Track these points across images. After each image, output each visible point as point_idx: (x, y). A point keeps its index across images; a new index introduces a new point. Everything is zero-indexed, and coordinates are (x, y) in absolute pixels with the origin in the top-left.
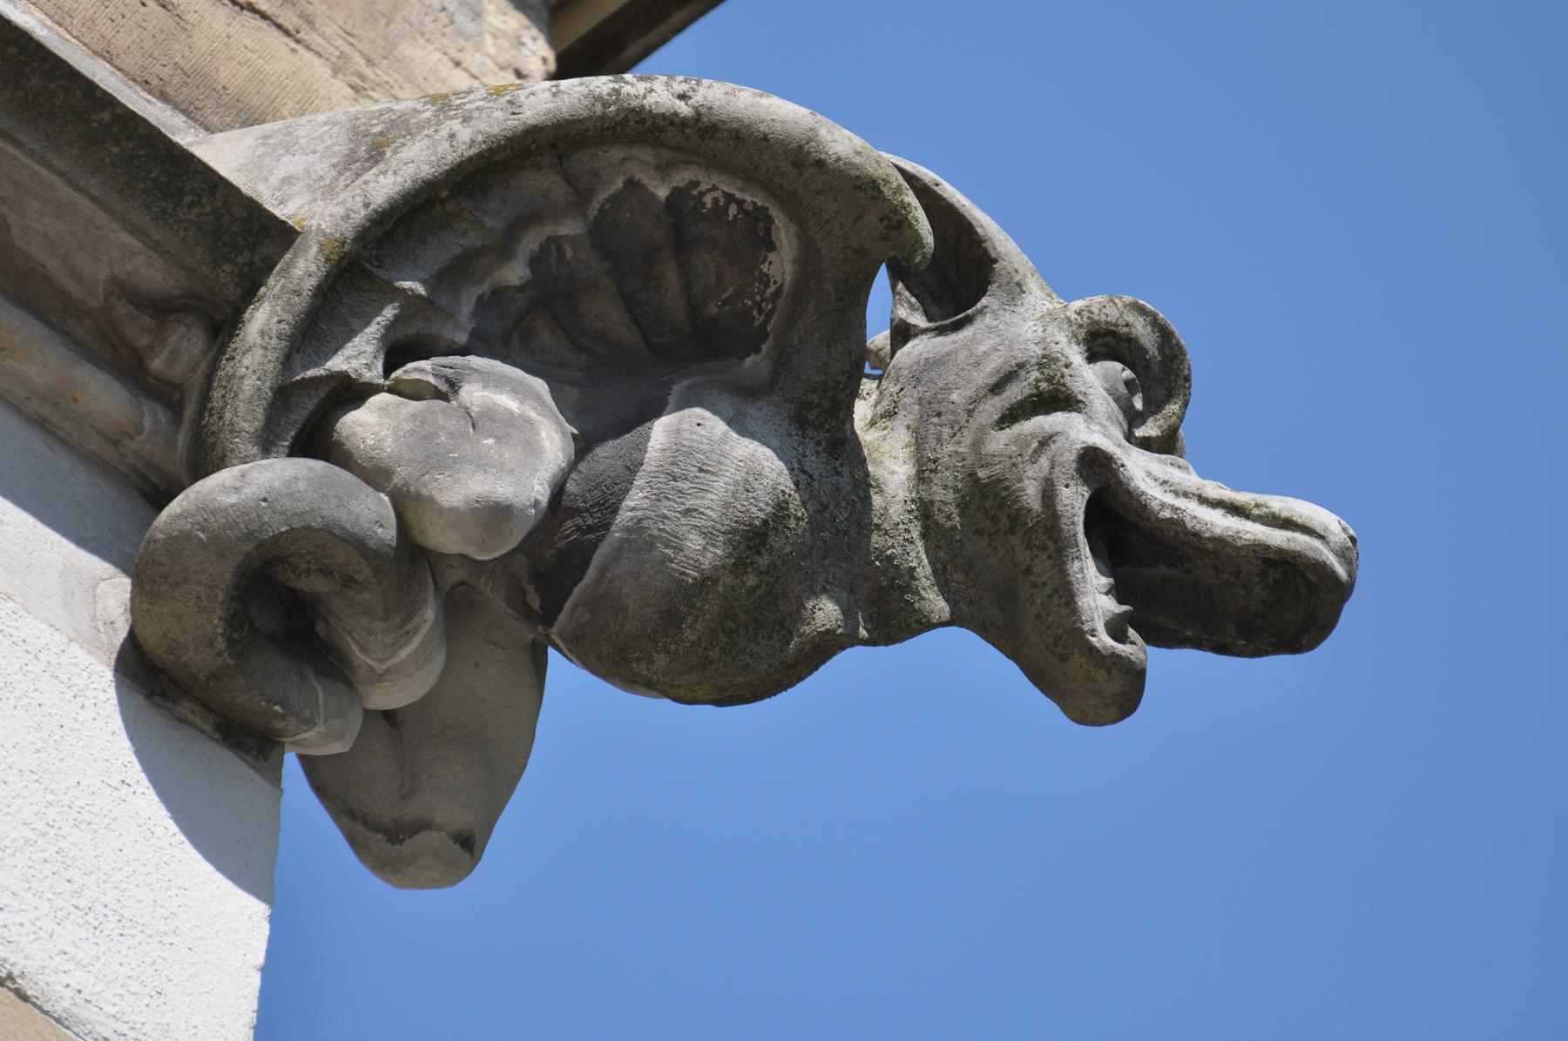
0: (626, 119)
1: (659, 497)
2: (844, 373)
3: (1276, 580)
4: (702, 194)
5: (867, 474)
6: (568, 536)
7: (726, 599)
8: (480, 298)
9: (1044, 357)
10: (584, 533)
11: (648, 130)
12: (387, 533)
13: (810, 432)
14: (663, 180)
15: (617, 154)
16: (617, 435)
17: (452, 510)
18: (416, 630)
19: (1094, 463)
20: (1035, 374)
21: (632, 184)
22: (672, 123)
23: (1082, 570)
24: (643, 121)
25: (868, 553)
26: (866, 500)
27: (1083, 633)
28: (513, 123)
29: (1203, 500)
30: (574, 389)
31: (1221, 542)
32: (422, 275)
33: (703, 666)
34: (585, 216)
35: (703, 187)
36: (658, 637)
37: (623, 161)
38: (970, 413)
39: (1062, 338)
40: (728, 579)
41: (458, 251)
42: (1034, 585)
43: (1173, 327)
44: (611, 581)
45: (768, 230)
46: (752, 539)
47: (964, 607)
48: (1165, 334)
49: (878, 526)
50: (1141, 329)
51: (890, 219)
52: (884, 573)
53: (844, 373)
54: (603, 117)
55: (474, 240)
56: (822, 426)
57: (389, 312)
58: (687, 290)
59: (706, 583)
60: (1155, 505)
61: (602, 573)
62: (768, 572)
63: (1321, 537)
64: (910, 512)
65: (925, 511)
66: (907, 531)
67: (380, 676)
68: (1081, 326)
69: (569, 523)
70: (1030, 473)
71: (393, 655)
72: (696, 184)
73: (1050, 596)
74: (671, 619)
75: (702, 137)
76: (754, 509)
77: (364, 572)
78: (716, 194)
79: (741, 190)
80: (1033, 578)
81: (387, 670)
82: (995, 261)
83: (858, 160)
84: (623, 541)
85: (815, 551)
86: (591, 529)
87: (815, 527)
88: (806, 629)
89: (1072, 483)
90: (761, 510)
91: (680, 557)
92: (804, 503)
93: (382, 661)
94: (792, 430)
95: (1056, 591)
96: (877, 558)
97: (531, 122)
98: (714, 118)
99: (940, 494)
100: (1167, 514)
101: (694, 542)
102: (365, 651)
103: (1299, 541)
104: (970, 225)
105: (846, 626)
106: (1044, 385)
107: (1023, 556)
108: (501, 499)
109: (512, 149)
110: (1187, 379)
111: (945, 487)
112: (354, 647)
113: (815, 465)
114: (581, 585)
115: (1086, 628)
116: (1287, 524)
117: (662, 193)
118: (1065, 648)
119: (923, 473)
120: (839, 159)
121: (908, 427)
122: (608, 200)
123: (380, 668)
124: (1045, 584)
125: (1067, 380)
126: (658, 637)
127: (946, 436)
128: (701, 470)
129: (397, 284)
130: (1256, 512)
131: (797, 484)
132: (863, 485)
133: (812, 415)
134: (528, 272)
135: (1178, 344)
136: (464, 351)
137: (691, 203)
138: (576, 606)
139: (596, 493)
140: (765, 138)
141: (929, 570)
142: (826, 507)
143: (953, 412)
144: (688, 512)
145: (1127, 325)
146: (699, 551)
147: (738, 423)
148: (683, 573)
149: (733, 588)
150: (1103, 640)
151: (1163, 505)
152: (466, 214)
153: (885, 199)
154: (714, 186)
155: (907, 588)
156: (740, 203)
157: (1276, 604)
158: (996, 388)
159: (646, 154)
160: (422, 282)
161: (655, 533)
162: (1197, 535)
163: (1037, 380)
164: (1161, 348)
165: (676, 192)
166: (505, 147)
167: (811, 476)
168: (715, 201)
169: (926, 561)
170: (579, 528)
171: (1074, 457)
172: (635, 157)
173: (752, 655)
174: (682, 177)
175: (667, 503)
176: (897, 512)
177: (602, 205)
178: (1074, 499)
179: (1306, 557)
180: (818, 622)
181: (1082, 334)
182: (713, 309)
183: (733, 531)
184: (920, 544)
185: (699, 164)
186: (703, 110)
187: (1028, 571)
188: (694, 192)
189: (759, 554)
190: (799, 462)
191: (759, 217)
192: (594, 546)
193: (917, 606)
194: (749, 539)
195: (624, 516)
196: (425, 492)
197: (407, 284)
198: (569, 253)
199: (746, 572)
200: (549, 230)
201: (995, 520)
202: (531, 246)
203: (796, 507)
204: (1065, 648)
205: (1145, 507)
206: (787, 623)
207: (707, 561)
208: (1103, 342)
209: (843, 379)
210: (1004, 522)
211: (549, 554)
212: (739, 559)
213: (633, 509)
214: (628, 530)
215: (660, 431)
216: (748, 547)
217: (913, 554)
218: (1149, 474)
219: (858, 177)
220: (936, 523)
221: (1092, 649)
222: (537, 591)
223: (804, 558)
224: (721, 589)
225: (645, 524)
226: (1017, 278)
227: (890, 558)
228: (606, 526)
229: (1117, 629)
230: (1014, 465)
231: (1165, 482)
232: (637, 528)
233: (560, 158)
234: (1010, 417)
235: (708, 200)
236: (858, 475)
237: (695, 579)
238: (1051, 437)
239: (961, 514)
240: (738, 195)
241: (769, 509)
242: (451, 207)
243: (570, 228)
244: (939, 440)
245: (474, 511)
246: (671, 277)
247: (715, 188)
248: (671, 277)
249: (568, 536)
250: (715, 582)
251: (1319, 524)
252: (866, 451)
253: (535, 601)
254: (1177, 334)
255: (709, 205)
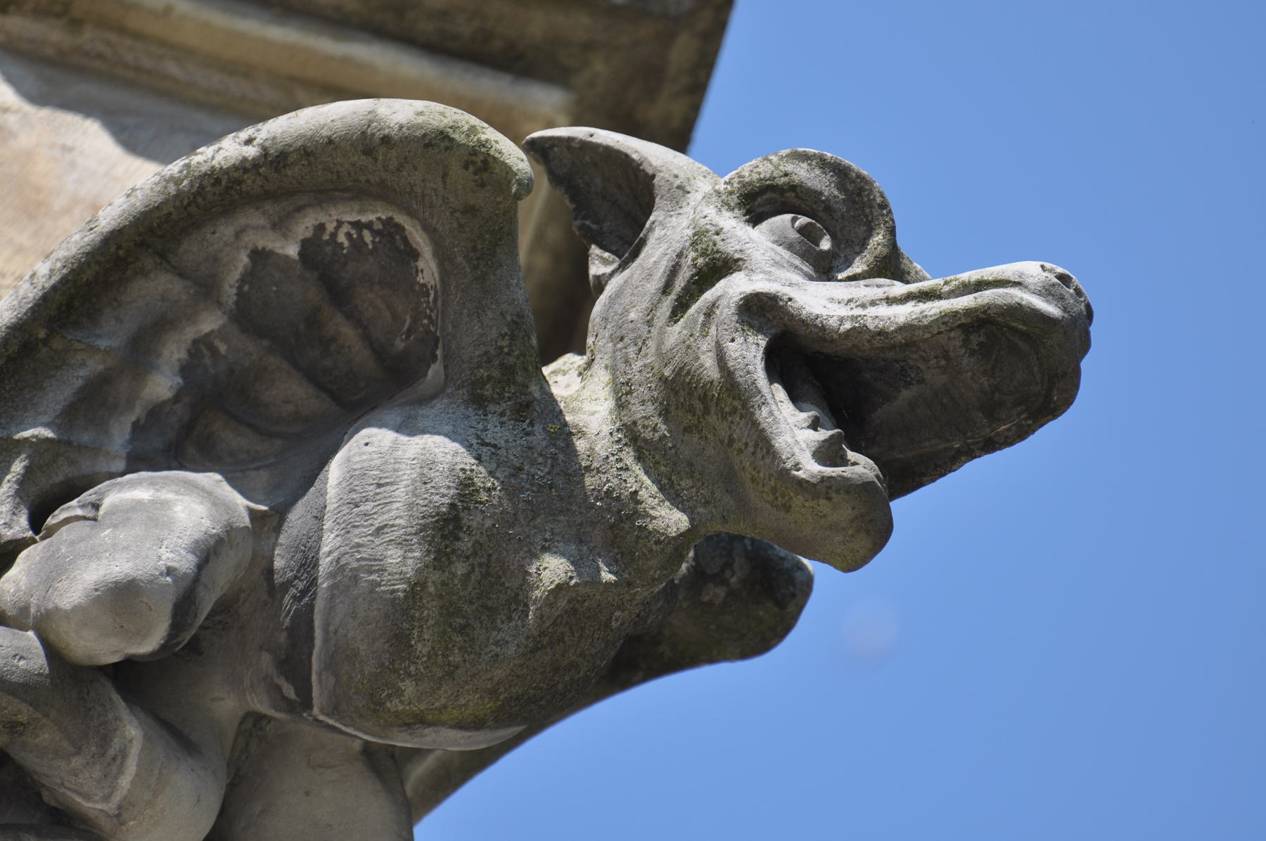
0: (202, 187)
1: (347, 529)
2: (503, 336)
3: (981, 344)
4: (334, 235)
5: (566, 424)
6: (289, 611)
7: (441, 597)
8: (135, 425)
9: (695, 235)
10: (300, 599)
11: (228, 188)
12: (37, 661)
13: (491, 408)
14: (285, 236)
15: (226, 230)
16: (304, 494)
17: (76, 609)
18: (124, 754)
19: (758, 310)
20: (692, 254)
21: (260, 256)
22: (246, 170)
23: (771, 413)
24: (218, 181)
25: (586, 497)
26: (570, 450)
27: (788, 471)
28: (90, 237)
29: (890, 301)
30: (261, 472)
31: (907, 328)
32: (45, 419)
33: (450, 674)
34: (219, 304)
35: (330, 227)
36: (397, 666)
37: (238, 235)
38: (649, 323)
39: (711, 211)
40: (436, 576)
41: (80, 383)
42: (740, 451)
43: (847, 162)
44: (336, 632)
45: (405, 240)
46: (446, 528)
47: (701, 510)
48: (840, 172)
49: (588, 469)
50: (802, 173)
51: (473, 163)
52: (609, 510)
53: (503, 336)
54: (179, 195)
55: (94, 366)
56: (501, 396)
57: (18, 467)
58: (367, 338)
59: (416, 589)
60: (833, 323)
61: (326, 631)
62: (475, 554)
63: (1017, 284)
64: (619, 441)
65: (631, 435)
66: (620, 460)
67: (118, 816)
68: (731, 193)
69: (287, 597)
70: (704, 348)
71: (113, 788)
72: (321, 228)
73: (753, 453)
74: (400, 641)
75: (277, 170)
76: (436, 498)
77: (25, 713)
78: (345, 228)
79: (362, 211)
80: (736, 445)
81: (120, 807)
82: (653, 176)
83: (420, 119)
84: (333, 587)
85: (521, 517)
86: (304, 593)
87: (511, 491)
88: (537, 593)
89: (736, 335)
90: (444, 496)
91: (386, 577)
92: (491, 473)
93: (106, 799)
94: (470, 411)
95: (756, 446)
96: (597, 499)
97: (108, 228)
98: (279, 147)
99: (643, 410)
100: (848, 326)
101: (394, 556)
102: (87, 797)
103: (987, 296)
104: (627, 156)
105: (580, 575)
106: (700, 261)
107: (723, 429)
108: (120, 577)
109: (98, 263)
110: (884, 205)
111: (643, 403)
112: (78, 799)
113: (497, 433)
114: (316, 651)
115: (789, 465)
116: (980, 285)
117: (292, 251)
118: (783, 496)
119: (622, 395)
120: (401, 127)
121: (606, 367)
122: (243, 280)
123: (110, 807)
124: (746, 445)
125: (721, 246)
126: (397, 666)
127: (632, 355)
128: (379, 486)
129: (17, 436)
130: (946, 288)
131: (478, 458)
132: (563, 435)
133: (488, 391)
134: (179, 380)
135: (859, 176)
136: (122, 474)
137: (328, 249)
138: (319, 675)
139: (299, 556)
140: (330, 141)
141: (654, 489)
142: (520, 469)
143: (633, 330)
144: (379, 531)
145: (786, 175)
146: (400, 562)
147: (408, 427)
148: (393, 591)
149: (443, 584)
150: (811, 468)
151: (842, 320)
152: (77, 345)
153: (459, 145)
154: (340, 220)
155: (636, 514)
156: (369, 226)
157: (1012, 372)
158: (666, 289)
159: (253, 218)
160: (46, 425)
161: (355, 565)
162: (882, 333)
163: (694, 260)
164: (841, 187)
165: (306, 244)
166: (88, 264)
167: (495, 446)
168: (348, 235)
169: (648, 482)
170: (294, 597)
171: (733, 310)
172: (248, 226)
173: (496, 643)
174: (304, 226)
175: (357, 531)
176: (603, 447)
177: (239, 288)
178: (748, 352)
179: (996, 306)
180: (546, 581)
181: (734, 200)
182: (400, 345)
183: (424, 528)
184: (637, 469)
185: (309, 205)
186: (267, 144)
187: (731, 441)
188: (326, 237)
189: (458, 539)
190: (478, 437)
191: (390, 231)
192: (311, 607)
193: (650, 527)
194: (441, 529)
195: (325, 564)
196: (50, 606)
197: (26, 434)
198: (223, 348)
199: (451, 563)
200: (190, 333)
201: (691, 410)
202: (176, 356)
203: (482, 477)
204: (783, 496)
205: (823, 328)
206: (521, 598)
207: (409, 571)
208: (758, 202)
209: (505, 343)
210: (698, 406)
211: (282, 638)
212: (438, 551)
213: (330, 553)
214: (332, 575)
215: (335, 471)
216: (444, 537)
217: (631, 480)
218: (832, 300)
219: (425, 135)
220: (645, 440)
221: (801, 483)
222: (287, 680)
223: (511, 526)
224: (432, 589)
225: (343, 561)
226: (677, 182)
227: (609, 493)
228: (313, 582)
229: (828, 454)
230: (689, 347)
231: (850, 301)
232: (339, 568)
233: (162, 255)
234: (680, 307)
235: (342, 238)
236: (552, 428)
237: (405, 591)
238: (714, 305)
239: (666, 421)
240: (364, 219)
241: (452, 492)
242: (57, 344)
243: (210, 322)
244: (627, 362)
245: (97, 600)
246: (348, 332)
247: (340, 223)
248: (348, 332)
249: (289, 611)
250: (423, 585)
251: (1025, 279)
252: (562, 405)
253: (289, 691)
254: (854, 166)
255: (346, 244)
